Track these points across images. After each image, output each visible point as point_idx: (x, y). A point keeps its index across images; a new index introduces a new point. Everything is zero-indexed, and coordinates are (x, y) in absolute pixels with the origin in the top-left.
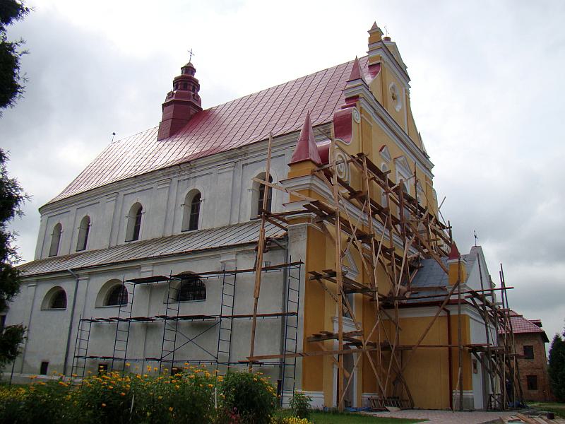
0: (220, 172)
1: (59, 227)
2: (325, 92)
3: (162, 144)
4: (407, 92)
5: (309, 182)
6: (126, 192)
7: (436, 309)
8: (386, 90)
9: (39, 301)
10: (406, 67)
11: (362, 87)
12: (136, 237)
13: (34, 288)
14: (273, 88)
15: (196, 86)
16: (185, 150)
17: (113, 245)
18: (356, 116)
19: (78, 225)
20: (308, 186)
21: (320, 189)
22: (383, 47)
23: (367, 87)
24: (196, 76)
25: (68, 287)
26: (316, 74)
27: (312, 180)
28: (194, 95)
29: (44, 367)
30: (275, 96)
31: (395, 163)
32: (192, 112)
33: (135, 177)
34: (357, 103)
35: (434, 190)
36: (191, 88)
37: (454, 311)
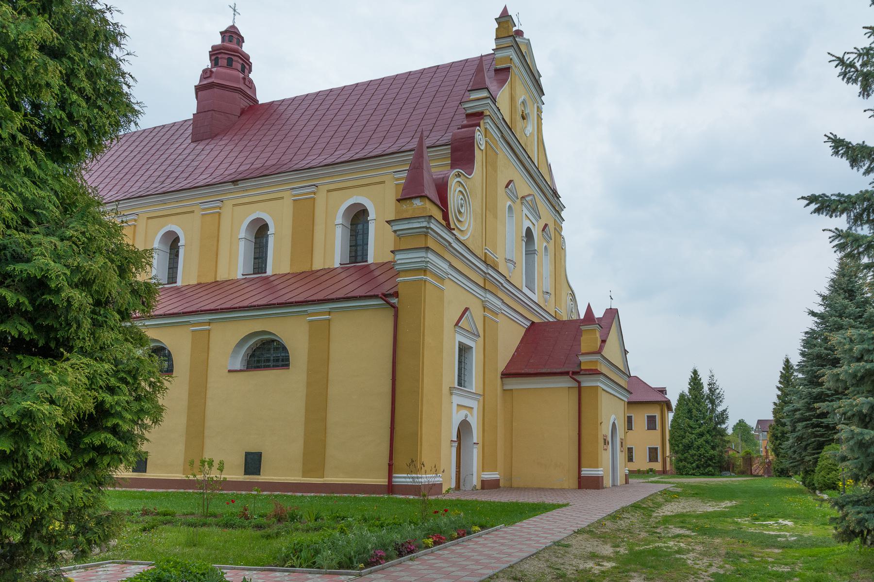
3: (200, 147)
5: (425, 224)
7: (567, 378)
8: (515, 107)
10: (540, 76)
15: (246, 64)
20: (425, 230)
22: (515, 46)
24: (246, 48)
26: (294, 99)
28: (244, 79)
32: (244, 103)
34: (482, 122)
36: (239, 67)
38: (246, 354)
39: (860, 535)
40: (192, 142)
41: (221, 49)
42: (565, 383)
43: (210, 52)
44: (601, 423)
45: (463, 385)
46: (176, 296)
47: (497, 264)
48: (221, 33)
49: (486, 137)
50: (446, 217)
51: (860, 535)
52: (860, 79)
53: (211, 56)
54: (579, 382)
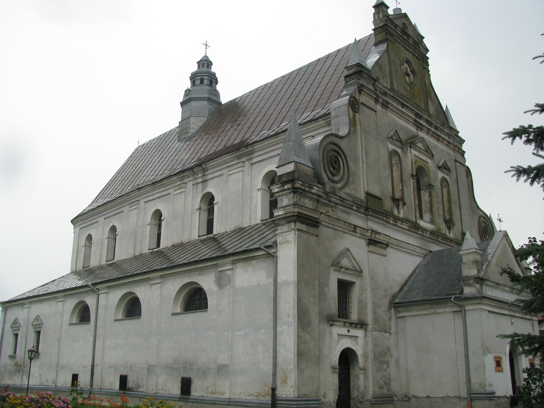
0: (230, 173)
1: (90, 237)
3: (182, 144)
6: (146, 200)
9: (67, 317)
12: (158, 245)
13: (62, 303)
14: (152, 139)
15: (213, 80)
19: (106, 235)
24: (214, 69)
25: (90, 301)
29: (47, 381)
30: (306, 76)
35: (468, 172)
38: (187, 294)
39: (533, 353)
40: (178, 142)
41: (196, 74)
43: (190, 77)
46: (164, 260)
48: (198, 63)
51: (533, 353)
52: (535, 172)
53: (191, 80)
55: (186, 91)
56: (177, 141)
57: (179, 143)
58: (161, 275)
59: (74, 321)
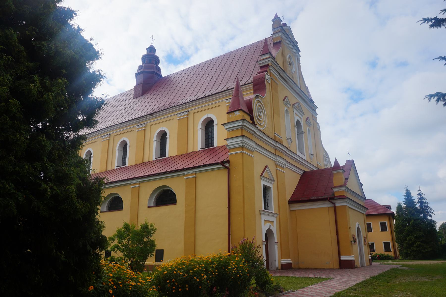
2: (245, 62)
3: (137, 100)
4: (299, 60)
5: (241, 124)
7: (327, 202)
11: (271, 59)
12: (124, 163)
16: (154, 104)
17: (109, 169)
18: (267, 77)
21: (250, 129)
23: (273, 58)
24: (157, 54)
27: (243, 122)
28: (156, 67)
31: (293, 108)
33: (121, 123)
35: (318, 124)
37: (339, 204)
42: (325, 205)
44: (350, 228)
45: (267, 208)
47: (282, 142)
49: (271, 77)
50: (252, 119)
54: (334, 204)
55: (139, 67)
56: (133, 98)
57: (134, 100)
58: (139, 181)
59: (152, 205)
